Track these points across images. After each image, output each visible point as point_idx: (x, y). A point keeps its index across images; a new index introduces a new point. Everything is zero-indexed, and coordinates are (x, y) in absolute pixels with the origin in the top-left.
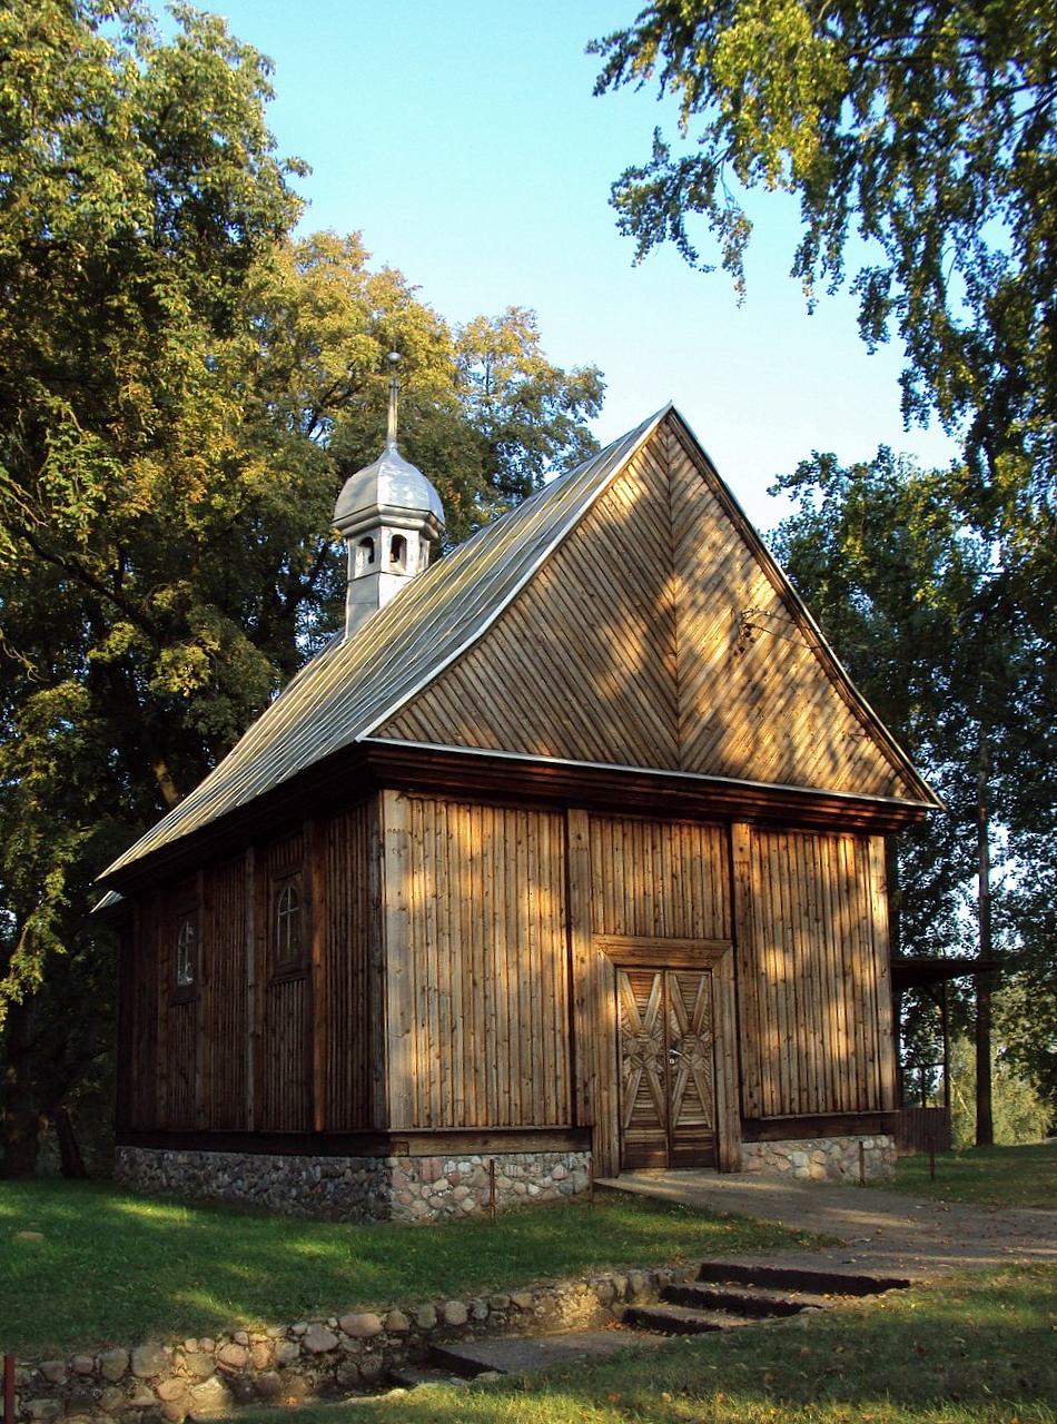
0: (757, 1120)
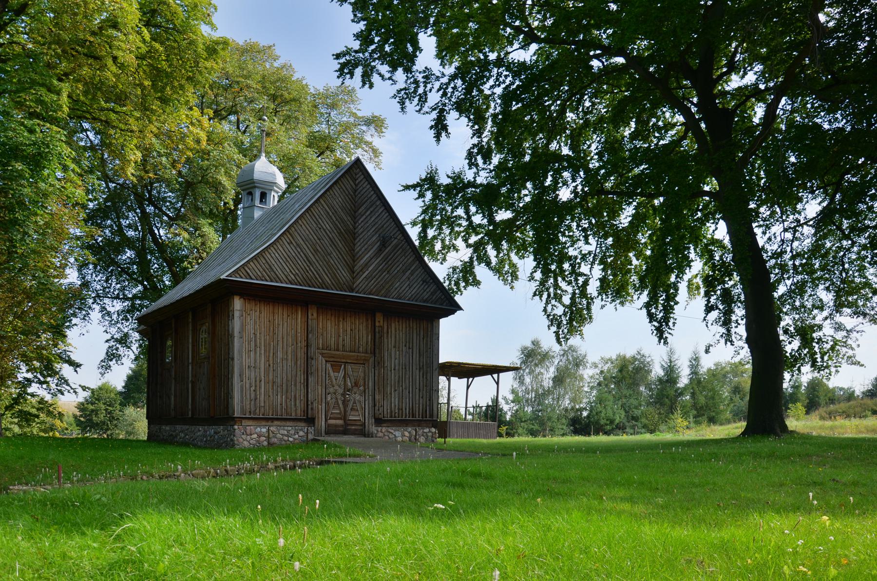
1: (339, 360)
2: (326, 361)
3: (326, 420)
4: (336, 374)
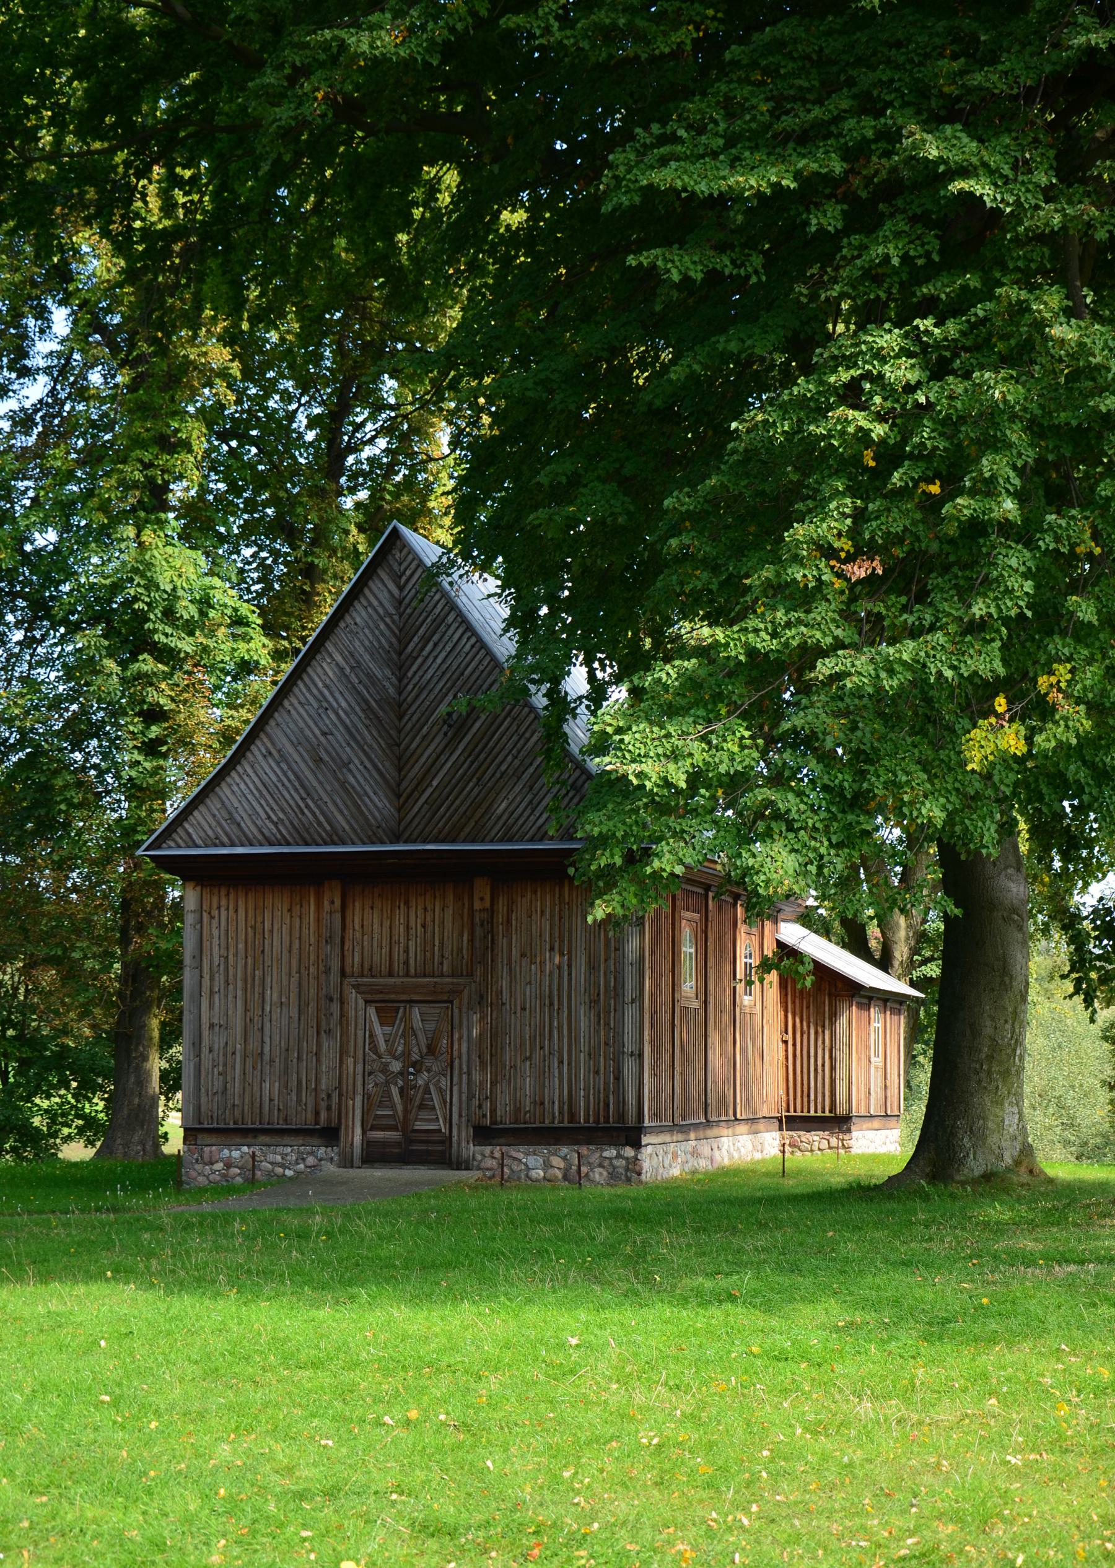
0: (486, 1127)
1: (393, 997)
2: (366, 1002)
3: (364, 1132)
4: (388, 1029)
